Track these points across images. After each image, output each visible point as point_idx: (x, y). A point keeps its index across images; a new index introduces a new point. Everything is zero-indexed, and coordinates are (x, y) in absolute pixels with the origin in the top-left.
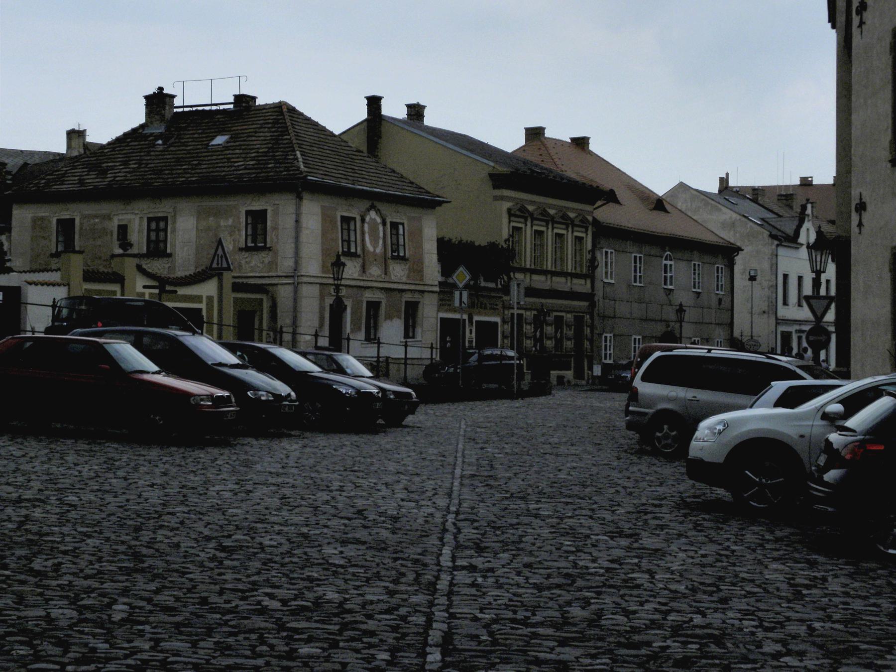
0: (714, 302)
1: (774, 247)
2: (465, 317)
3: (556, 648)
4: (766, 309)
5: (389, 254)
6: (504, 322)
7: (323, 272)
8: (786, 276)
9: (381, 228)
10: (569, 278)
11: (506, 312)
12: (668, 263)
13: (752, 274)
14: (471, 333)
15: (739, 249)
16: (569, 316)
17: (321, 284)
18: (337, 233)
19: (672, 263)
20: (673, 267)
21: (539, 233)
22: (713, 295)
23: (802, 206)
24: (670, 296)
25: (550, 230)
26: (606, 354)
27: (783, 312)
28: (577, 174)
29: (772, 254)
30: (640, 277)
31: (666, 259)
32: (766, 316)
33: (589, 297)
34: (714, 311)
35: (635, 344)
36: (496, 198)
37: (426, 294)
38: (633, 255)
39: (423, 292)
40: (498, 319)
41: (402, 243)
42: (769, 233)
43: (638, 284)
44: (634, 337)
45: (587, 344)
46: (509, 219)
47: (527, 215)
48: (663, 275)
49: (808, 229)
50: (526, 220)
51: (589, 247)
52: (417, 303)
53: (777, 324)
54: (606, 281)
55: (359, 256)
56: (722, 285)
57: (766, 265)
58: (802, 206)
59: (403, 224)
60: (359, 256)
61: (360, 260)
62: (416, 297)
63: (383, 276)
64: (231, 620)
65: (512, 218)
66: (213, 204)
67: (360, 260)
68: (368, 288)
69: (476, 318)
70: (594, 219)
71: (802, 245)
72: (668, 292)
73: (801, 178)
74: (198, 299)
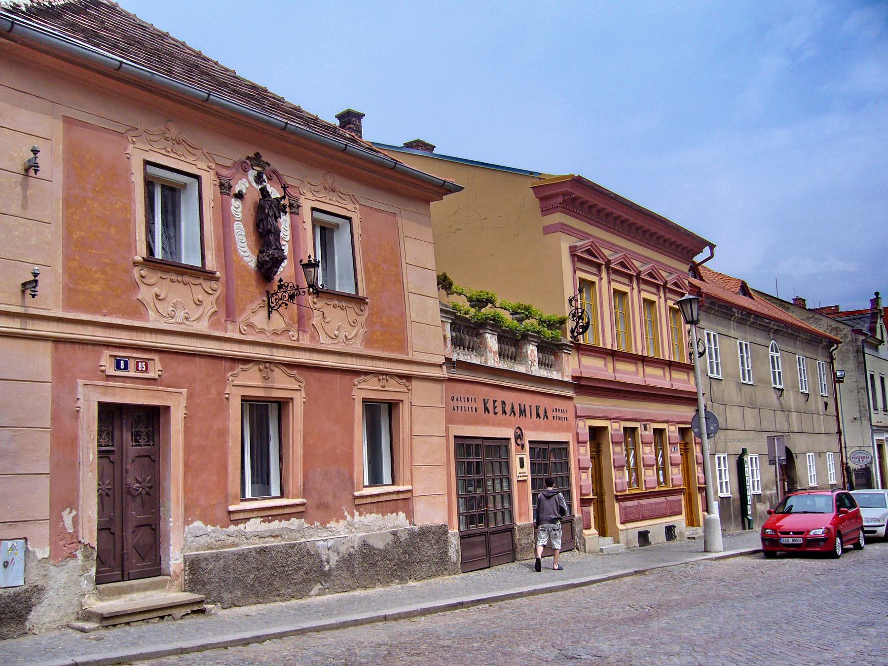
0: (821, 406)
4: (857, 415)
8: (872, 376)
10: (667, 369)
11: (581, 424)
14: (522, 466)
19: (779, 354)
21: (650, 303)
25: (662, 300)
29: (857, 351)
32: (858, 423)
34: (822, 417)
36: (548, 230)
37: (415, 383)
38: (705, 332)
39: (408, 378)
43: (747, 382)
44: (807, 454)
45: (698, 471)
46: (574, 265)
47: (600, 261)
48: (771, 370)
49: (881, 326)
52: (392, 406)
53: (873, 431)
54: (712, 376)
55: (210, 276)
56: (779, 373)
60: (210, 276)
61: (219, 287)
62: (392, 390)
65: (579, 265)
66: (181, 484)
67: (219, 287)
69: (530, 436)
72: (779, 393)
73: (442, 199)
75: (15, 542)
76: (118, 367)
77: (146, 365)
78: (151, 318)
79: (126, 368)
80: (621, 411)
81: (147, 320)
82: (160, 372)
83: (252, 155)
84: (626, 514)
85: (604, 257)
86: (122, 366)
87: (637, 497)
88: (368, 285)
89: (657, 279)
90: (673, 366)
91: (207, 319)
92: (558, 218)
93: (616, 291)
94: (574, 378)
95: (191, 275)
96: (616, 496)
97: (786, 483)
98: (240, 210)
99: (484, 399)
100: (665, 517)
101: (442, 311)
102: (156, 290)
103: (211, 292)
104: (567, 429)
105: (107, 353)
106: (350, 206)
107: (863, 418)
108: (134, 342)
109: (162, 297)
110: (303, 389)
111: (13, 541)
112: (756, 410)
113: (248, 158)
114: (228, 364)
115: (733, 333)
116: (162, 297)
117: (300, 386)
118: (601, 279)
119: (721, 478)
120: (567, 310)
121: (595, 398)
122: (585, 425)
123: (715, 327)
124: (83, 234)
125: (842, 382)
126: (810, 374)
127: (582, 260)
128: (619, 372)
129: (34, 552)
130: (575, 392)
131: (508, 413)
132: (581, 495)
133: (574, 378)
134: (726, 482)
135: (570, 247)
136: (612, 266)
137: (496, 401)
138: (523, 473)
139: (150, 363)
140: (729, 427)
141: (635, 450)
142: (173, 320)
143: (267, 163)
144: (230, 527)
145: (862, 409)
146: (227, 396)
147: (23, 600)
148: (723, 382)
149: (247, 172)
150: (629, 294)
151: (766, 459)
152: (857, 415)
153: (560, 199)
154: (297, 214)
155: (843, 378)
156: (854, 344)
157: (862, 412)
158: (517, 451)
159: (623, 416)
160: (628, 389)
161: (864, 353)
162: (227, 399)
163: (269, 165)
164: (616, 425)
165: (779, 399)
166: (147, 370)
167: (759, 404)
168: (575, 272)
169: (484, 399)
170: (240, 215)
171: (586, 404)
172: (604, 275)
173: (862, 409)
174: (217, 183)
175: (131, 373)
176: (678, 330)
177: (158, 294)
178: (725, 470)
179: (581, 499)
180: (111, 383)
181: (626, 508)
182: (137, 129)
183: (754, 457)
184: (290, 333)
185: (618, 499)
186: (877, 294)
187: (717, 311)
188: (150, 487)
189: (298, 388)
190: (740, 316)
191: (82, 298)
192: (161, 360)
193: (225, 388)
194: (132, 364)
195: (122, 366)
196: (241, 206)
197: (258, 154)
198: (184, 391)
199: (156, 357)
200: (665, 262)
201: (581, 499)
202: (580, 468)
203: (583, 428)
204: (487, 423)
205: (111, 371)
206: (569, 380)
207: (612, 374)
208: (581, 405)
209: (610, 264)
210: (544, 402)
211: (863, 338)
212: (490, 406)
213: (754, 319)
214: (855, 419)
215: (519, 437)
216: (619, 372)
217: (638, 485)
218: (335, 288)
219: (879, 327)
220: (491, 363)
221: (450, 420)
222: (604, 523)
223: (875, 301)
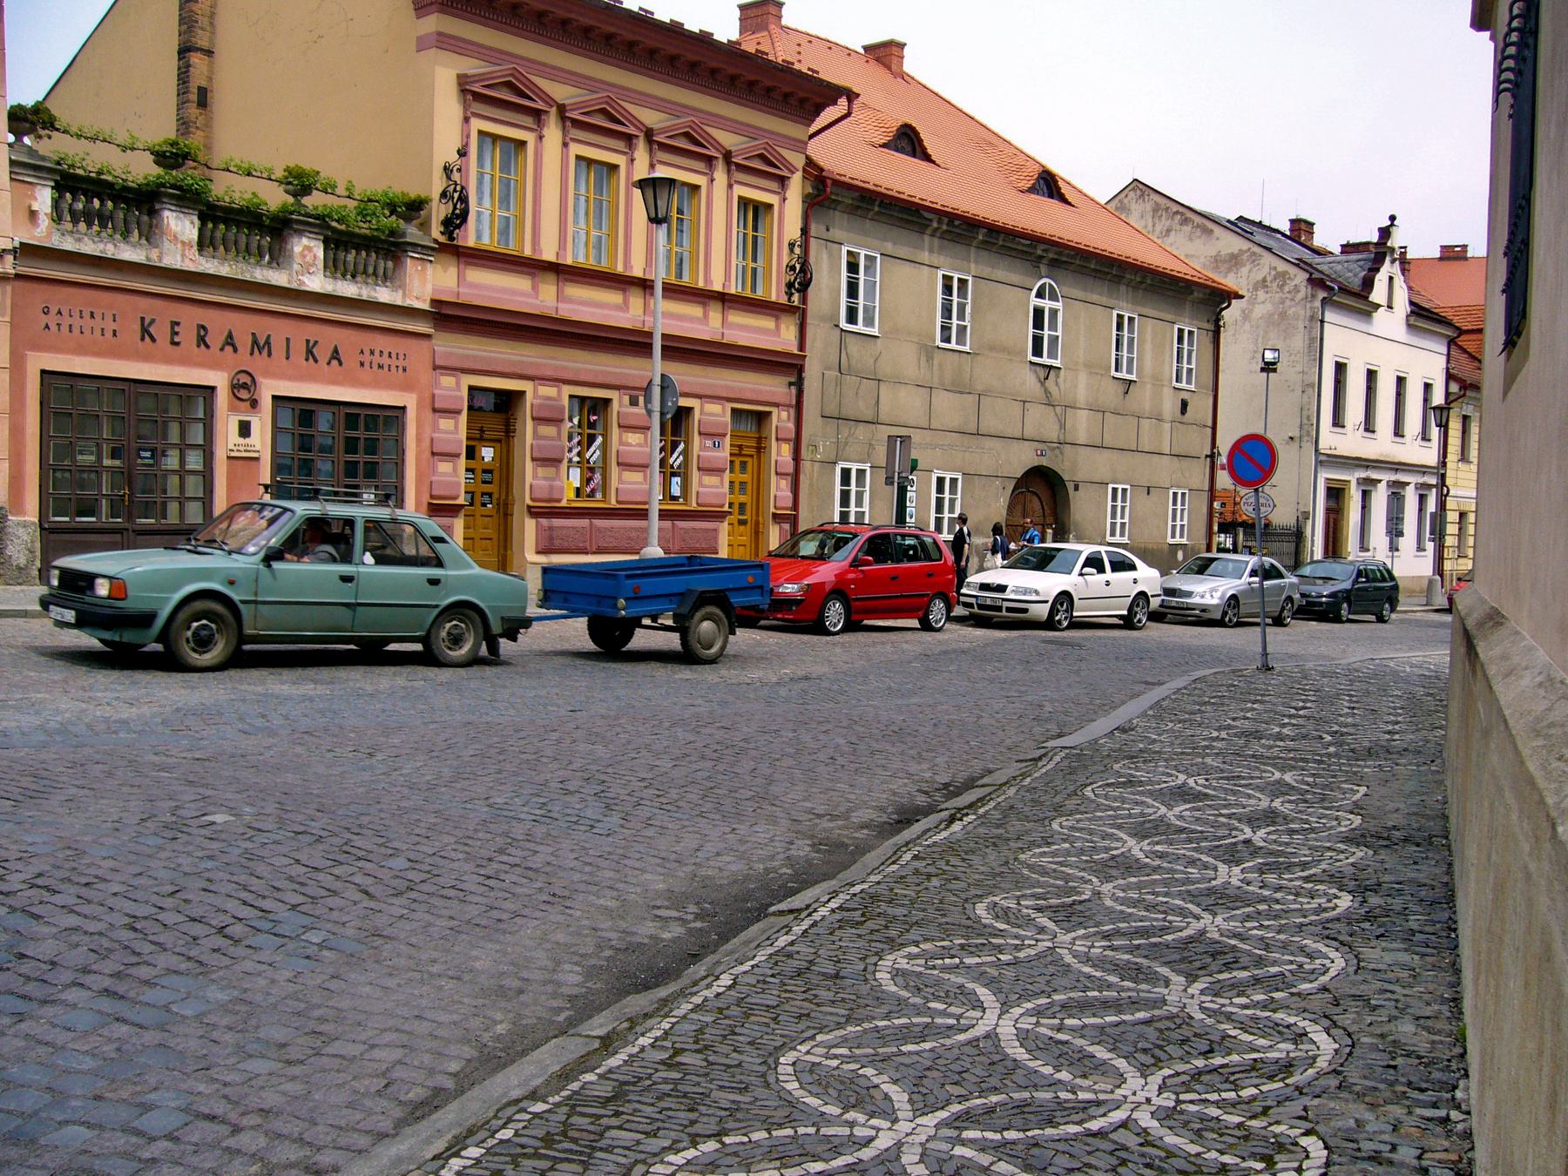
0: (1170, 406)
1: (1318, 304)
2: (219, 379)
4: (1295, 433)
8: (1340, 368)
11: (447, 381)
12: (1047, 304)
13: (1269, 356)
15: (1229, 296)
16: (714, 408)
19: (1058, 305)
20: (1060, 315)
22: (1167, 393)
23: (1380, 230)
24: (1050, 383)
26: (1113, 525)
27: (1330, 440)
29: (1312, 318)
30: (1190, 371)
31: (1040, 295)
32: (1296, 445)
33: (790, 366)
34: (1167, 426)
35: (1175, 503)
40: (409, 400)
42: (1307, 276)
44: (1111, 486)
46: (465, 109)
48: (1031, 330)
49: (1391, 279)
51: (793, 230)
53: (1319, 463)
57: (1299, 341)
58: (1380, 230)
64: (1255, 928)
65: (576, 133)
69: (269, 388)
70: (810, 162)
71: (1378, 306)
72: (1042, 373)
80: (565, 368)
84: (551, 538)
85: (717, 144)
87: (589, 514)
89: (624, 124)
90: (731, 301)
93: (744, 203)
94: (435, 302)
96: (529, 507)
97: (1050, 531)
100: (587, 553)
104: (407, 387)
107: (1305, 439)
112: (970, 400)
115: (925, 256)
119: (1174, 519)
120: (438, 185)
121: (499, 341)
122: (458, 384)
123: (876, 243)
125: (1275, 370)
126: (1148, 347)
127: (478, 97)
128: (570, 301)
130: (436, 327)
131: (323, 360)
132: (432, 497)
133: (435, 302)
134: (1182, 526)
135: (459, 76)
136: (660, 138)
137: (178, 324)
140: (882, 418)
141: (605, 436)
145: (1305, 421)
148: (879, 341)
150: (776, 208)
151: (882, 475)
152: (1295, 433)
155: (1274, 364)
156: (1308, 305)
157: (1306, 427)
158: (232, 409)
159: (566, 376)
160: (641, 340)
161: (1322, 321)
164: (548, 391)
165: (1042, 384)
167: (979, 388)
169: (143, 319)
172: (720, 175)
173: (1305, 421)
178: (1182, 510)
179: (430, 504)
181: (551, 528)
183: (1180, 492)
185: (534, 513)
186: (1393, 218)
187: (878, 213)
190: (945, 227)
200: (766, 127)
201: (430, 504)
202: (433, 454)
203: (455, 389)
204: (147, 358)
206: (426, 306)
207: (554, 304)
208: (443, 349)
209: (652, 135)
211: (1325, 295)
213: (985, 235)
214: (1291, 438)
215: (244, 389)
216: (570, 301)
217: (604, 495)
218: (697, 283)
219: (1386, 280)
220: (173, 258)
222: (506, 548)
223: (1385, 233)
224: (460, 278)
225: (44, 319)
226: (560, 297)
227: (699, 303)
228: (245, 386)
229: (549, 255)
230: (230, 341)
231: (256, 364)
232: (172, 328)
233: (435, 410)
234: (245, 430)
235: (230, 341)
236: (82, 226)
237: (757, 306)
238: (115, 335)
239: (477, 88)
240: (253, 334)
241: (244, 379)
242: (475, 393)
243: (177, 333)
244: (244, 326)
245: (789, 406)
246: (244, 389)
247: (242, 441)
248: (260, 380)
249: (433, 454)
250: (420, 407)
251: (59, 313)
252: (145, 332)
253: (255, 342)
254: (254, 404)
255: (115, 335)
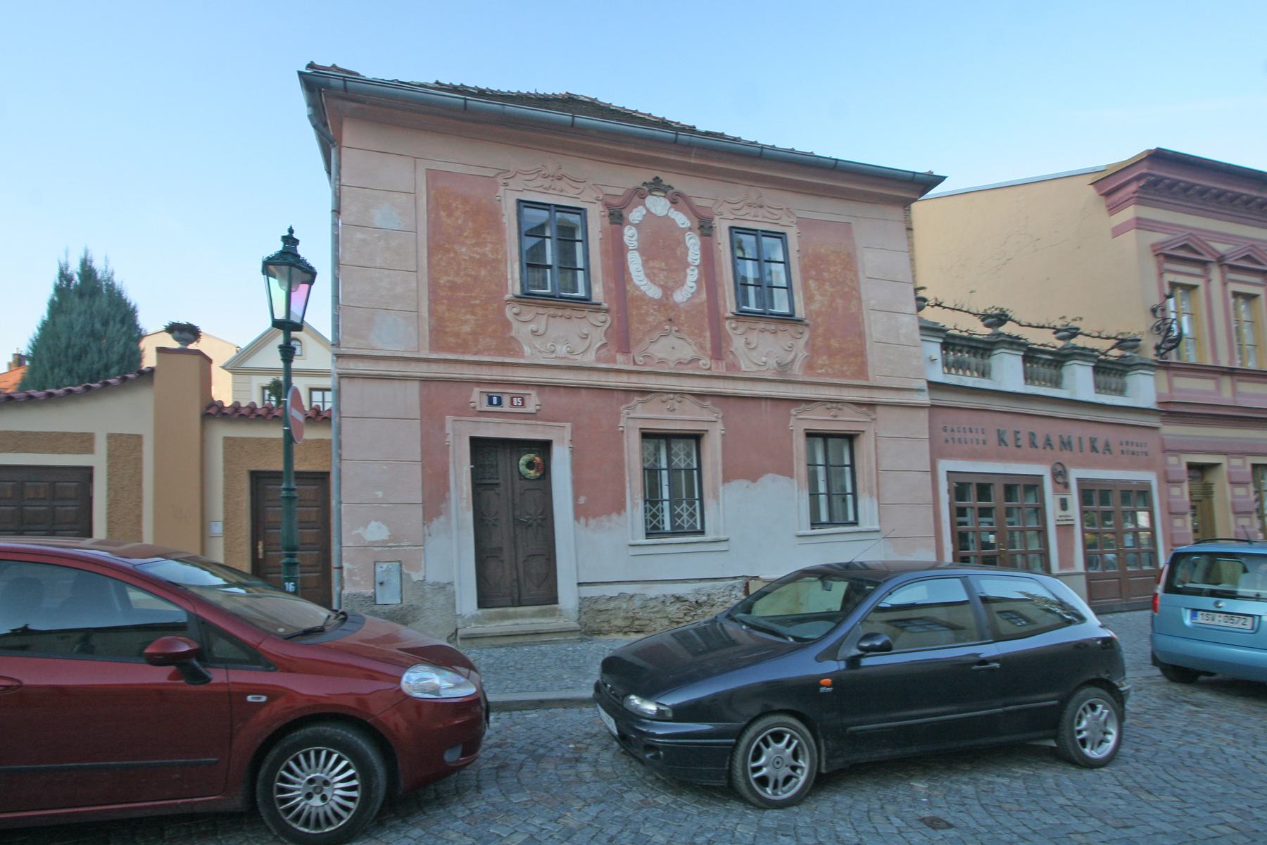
2: (1043, 470)
3: (1048, 377)
5: (729, 305)
6: (1168, 481)
7: (435, 346)
9: (693, 244)
11: (1172, 460)
17: (425, 381)
18: (501, 240)
28: (1021, 593)
37: (879, 409)
39: (871, 405)
40: (1150, 477)
41: (783, 282)
50: (1207, 271)
55: (597, 308)
59: (780, 236)
60: (597, 308)
62: (845, 421)
63: (705, 362)
65: (1168, 266)
68: (644, 392)
74: (84, 442)
75: (390, 565)
76: (491, 403)
77: (523, 400)
78: (526, 354)
79: (500, 403)
81: (523, 356)
82: (538, 407)
83: (649, 180)
86: (495, 401)
88: (806, 304)
91: (594, 353)
92: (1129, 213)
95: (573, 308)
98: (635, 238)
99: (999, 430)
101: (922, 328)
102: (532, 326)
103: (601, 324)
104: (1148, 467)
105: (477, 390)
106: (785, 220)
108: (505, 378)
109: (540, 332)
110: (720, 421)
111: (387, 564)
113: (645, 184)
114: (622, 396)
116: (540, 332)
117: (717, 417)
118: (1209, 281)
122: (1179, 460)
124: (450, 278)
129: (409, 575)
130: (1162, 422)
136: (1230, 262)
137: (1018, 432)
138: (1067, 516)
139: (526, 398)
142: (554, 355)
143: (670, 187)
144: (370, 526)
146: (621, 429)
147: (399, 617)
149: (644, 198)
153: (1133, 187)
154: (709, 235)
162: (622, 432)
163: (672, 188)
164: (1236, 462)
166: (523, 405)
168: (1161, 275)
170: (636, 243)
171: (1172, 431)
174: (607, 212)
175: (506, 407)
176: (1236, 308)
177: (534, 329)
180: (483, 419)
182: (509, 171)
184: (701, 362)
188: (543, 520)
189: (714, 419)
191: (452, 340)
192: (538, 394)
193: (619, 422)
194: (506, 400)
195: (495, 401)
196: (636, 234)
197: (657, 178)
198: (568, 425)
199: (533, 393)
203: (1179, 464)
205: (485, 407)
210: (1103, 434)
212: (1009, 438)
215: (1060, 476)
221: (936, 454)
224: (1170, 383)
225: (944, 434)
226: (1235, 392)
227: (1212, 378)
228: (1060, 474)
229: (1224, 362)
230: (1048, 443)
231: (1065, 456)
232: (1015, 436)
233: (1231, 483)
234: (1064, 505)
235: (1048, 443)
236: (953, 371)
237: (1192, 370)
238: (984, 443)
239: (1167, 251)
240: (1061, 436)
241: (1059, 468)
242: (1259, 471)
243: (1019, 439)
244: (1056, 431)
245: (659, 443)
246: (1060, 476)
247: (1063, 513)
248: (1068, 468)
249: (1171, 513)
250: (1159, 482)
251: (953, 430)
252: (1002, 441)
253: (1062, 443)
254: (1066, 485)
255: (984, 443)
